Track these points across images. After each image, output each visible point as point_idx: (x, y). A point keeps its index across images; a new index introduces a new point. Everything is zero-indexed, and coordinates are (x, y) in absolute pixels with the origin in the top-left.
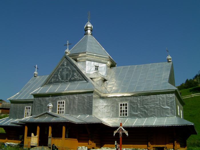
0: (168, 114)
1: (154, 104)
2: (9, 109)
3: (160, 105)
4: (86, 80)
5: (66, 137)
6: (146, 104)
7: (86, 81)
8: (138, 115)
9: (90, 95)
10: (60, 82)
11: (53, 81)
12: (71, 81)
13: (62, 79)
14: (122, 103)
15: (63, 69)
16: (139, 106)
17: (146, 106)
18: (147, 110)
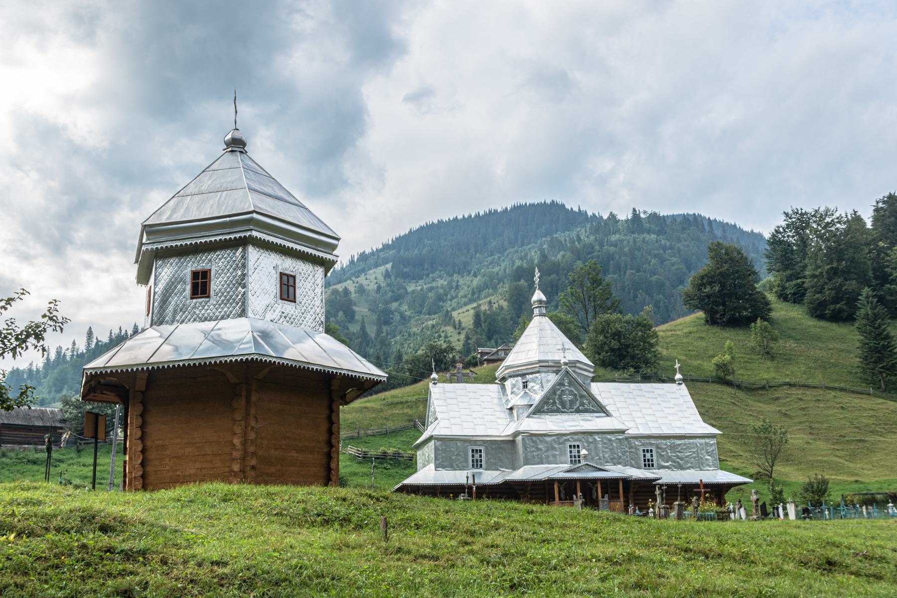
0: (710, 467)
1: (690, 452)
2: (338, 256)
3: (698, 455)
4: (606, 413)
5: (560, 499)
6: (679, 452)
7: (605, 415)
8: (670, 467)
9: (121, 485)
10: (559, 412)
11: (547, 409)
12: (578, 411)
13: (564, 407)
14: (646, 449)
15: (562, 391)
16: (670, 454)
17: (678, 454)
18: (682, 459)
